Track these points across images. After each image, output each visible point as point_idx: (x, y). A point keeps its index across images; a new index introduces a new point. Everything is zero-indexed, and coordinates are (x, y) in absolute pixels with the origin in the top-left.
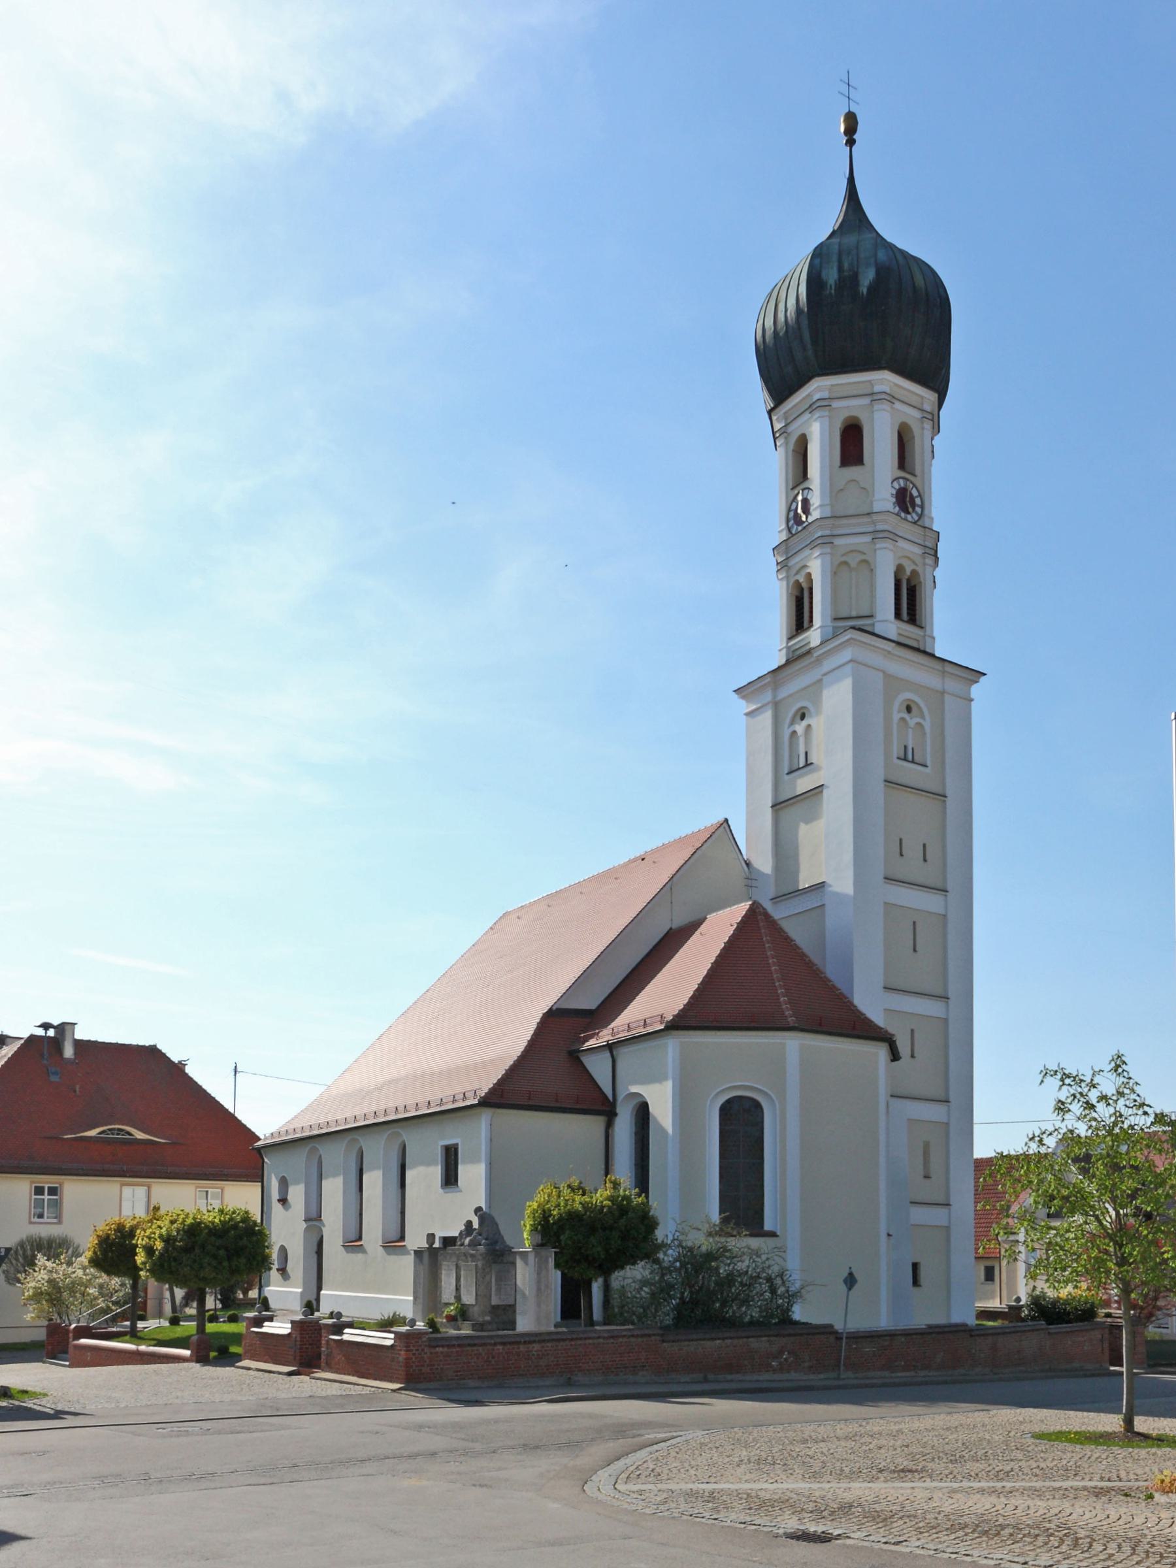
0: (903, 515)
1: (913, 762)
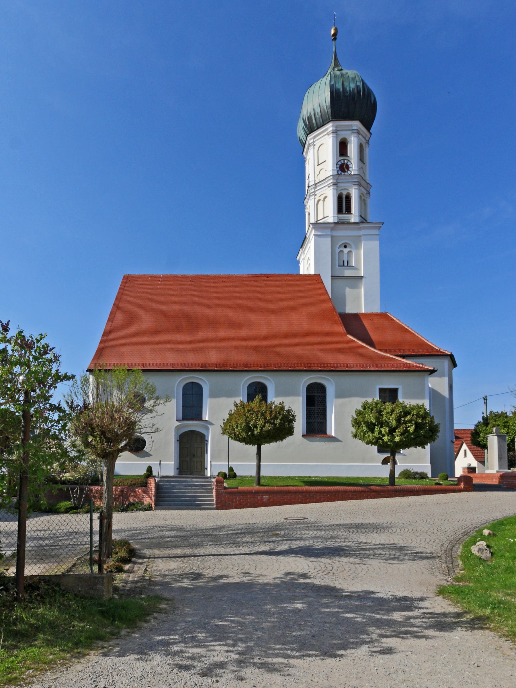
0: (343, 173)
1: (347, 266)
